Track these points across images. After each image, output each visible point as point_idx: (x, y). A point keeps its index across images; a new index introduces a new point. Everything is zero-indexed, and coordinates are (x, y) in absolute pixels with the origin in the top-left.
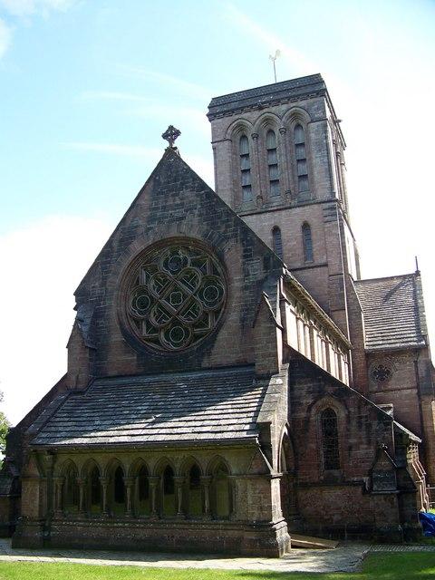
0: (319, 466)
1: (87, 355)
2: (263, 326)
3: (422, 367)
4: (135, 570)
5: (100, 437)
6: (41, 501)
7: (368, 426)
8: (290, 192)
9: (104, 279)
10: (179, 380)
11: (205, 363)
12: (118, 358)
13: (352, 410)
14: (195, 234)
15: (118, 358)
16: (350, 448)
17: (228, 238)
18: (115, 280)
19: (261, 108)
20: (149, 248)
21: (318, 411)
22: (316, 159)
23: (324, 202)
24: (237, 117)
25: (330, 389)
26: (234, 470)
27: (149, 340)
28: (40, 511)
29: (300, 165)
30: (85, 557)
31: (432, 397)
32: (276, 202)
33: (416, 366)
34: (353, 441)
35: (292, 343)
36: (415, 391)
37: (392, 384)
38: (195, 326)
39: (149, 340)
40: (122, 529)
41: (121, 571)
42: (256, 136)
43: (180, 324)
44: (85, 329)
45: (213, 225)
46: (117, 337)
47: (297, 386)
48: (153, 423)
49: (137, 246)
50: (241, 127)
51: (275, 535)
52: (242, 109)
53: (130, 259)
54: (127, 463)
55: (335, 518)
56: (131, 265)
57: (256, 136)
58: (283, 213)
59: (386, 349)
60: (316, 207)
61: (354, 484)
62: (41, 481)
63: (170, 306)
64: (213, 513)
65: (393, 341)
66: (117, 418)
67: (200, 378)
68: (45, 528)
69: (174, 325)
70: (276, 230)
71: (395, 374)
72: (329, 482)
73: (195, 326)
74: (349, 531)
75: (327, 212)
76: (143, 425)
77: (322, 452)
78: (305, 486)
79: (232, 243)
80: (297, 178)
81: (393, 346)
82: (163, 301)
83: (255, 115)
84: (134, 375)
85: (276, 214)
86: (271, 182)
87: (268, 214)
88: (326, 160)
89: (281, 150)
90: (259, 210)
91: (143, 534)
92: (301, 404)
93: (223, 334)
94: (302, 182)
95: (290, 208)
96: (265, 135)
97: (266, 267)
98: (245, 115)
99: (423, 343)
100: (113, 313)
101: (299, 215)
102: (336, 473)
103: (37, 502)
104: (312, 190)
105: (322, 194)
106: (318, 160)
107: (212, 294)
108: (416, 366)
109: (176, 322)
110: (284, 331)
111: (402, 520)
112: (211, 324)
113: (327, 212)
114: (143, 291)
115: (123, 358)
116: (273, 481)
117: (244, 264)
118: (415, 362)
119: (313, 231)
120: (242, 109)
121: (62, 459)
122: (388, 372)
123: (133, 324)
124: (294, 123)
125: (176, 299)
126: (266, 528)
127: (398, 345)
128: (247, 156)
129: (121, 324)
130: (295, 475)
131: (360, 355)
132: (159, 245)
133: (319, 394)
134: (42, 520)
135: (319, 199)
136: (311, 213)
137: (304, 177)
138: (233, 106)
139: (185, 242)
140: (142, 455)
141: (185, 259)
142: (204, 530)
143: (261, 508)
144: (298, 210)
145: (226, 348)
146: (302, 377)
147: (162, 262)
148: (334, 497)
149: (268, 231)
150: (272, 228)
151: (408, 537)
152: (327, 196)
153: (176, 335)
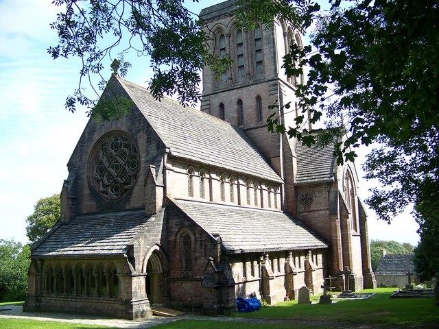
0: (181, 268)
1: (70, 202)
2: (150, 185)
3: (332, 195)
4: (25, 323)
5: (70, 251)
6: (36, 285)
7: (206, 246)
8: (249, 74)
9: (81, 156)
10: (112, 217)
11: (127, 207)
12: (88, 204)
13: (197, 236)
14: (124, 129)
15: (88, 204)
16: (196, 259)
17: (139, 131)
18: (86, 157)
19: (231, 15)
20: (102, 137)
21: (181, 236)
22: (266, 50)
23: (272, 80)
24: (216, 22)
25: (187, 223)
26: (118, 271)
27: (103, 193)
28: (36, 292)
29: (258, 54)
30: (37, 316)
31: (19, 265)
32: (241, 81)
33: (329, 195)
34: (197, 254)
35: (172, 195)
36: (328, 212)
37: (313, 207)
38: (124, 184)
39: (103, 193)
40: (72, 302)
41: (44, 323)
42: (229, 36)
43: (118, 183)
44: (69, 187)
45: (133, 123)
46: (87, 191)
47: (171, 221)
48: (88, 243)
49: (97, 137)
50: (219, 29)
51: (132, 308)
52: (219, 16)
53: (94, 143)
54: (73, 265)
55: (188, 299)
56: (94, 147)
57: (229, 36)
58: (244, 89)
59: (308, 183)
60: (265, 84)
61: (197, 280)
62: (36, 276)
63: (113, 172)
64: (111, 295)
65: (314, 177)
66: (73, 240)
67: (123, 216)
68: (38, 301)
69: (115, 184)
70: (240, 102)
71: (315, 200)
72: (186, 278)
73: (124, 184)
74: (194, 307)
75: (271, 88)
76: (82, 245)
77: (183, 261)
78: (174, 280)
79: (141, 133)
80: (255, 64)
81: (313, 180)
82: (110, 169)
83: (229, 19)
84: (94, 214)
85: (240, 91)
86: (239, 67)
87: (235, 91)
88: (272, 50)
89: (245, 45)
90: (229, 88)
91: (79, 305)
92: (172, 232)
93: (136, 189)
94: (259, 67)
95: (248, 86)
96: (235, 34)
97: (157, 149)
98: (222, 21)
99: (333, 178)
100: (85, 176)
101: (254, 90)
102: (190, 273)
103: (34, 287)
104: (263, 72)
105: (269, 75)
106: (267, 51)
107: (133, 165)
108: (329, 195)
109: (116, 182)
110: (165, 188)
111: (220, 302)
112: (133, 181)
113: (271, 88)
114: (101, 163)
115: (89, 203)
116: (135, 280)
117: (147, 147)
118: (329, 192)
119: (263, 101)
120: (219, 16)
121: (46, 263)
122: (311, 199)
123: (96, 183)
124: (220, 34)
125: (117, 168)
126: (128, 303)
127: (316, 180)
128: (224, 49)
129: (89, 183)
130: (168, 273)
131: (291, 188)
132: (107, 135)
133: (181, 226)
134: (37, 296)
135: (267, 78)
136: (262, 89)
137: (260, 62)
138: (214, 14)
139: (119, 133)
140: (79, 261)
141: (121, 143)
142: (105, 303)
143: (128, 293)
144: (253, 87)
145: (135, 201)
146: (173, 216)
147: (110, 145)
148: (186, 289)
149: (235, 102)
150: (236, 100)
151: (222, 311)
152: (273, 76)
153: (116, 189)
